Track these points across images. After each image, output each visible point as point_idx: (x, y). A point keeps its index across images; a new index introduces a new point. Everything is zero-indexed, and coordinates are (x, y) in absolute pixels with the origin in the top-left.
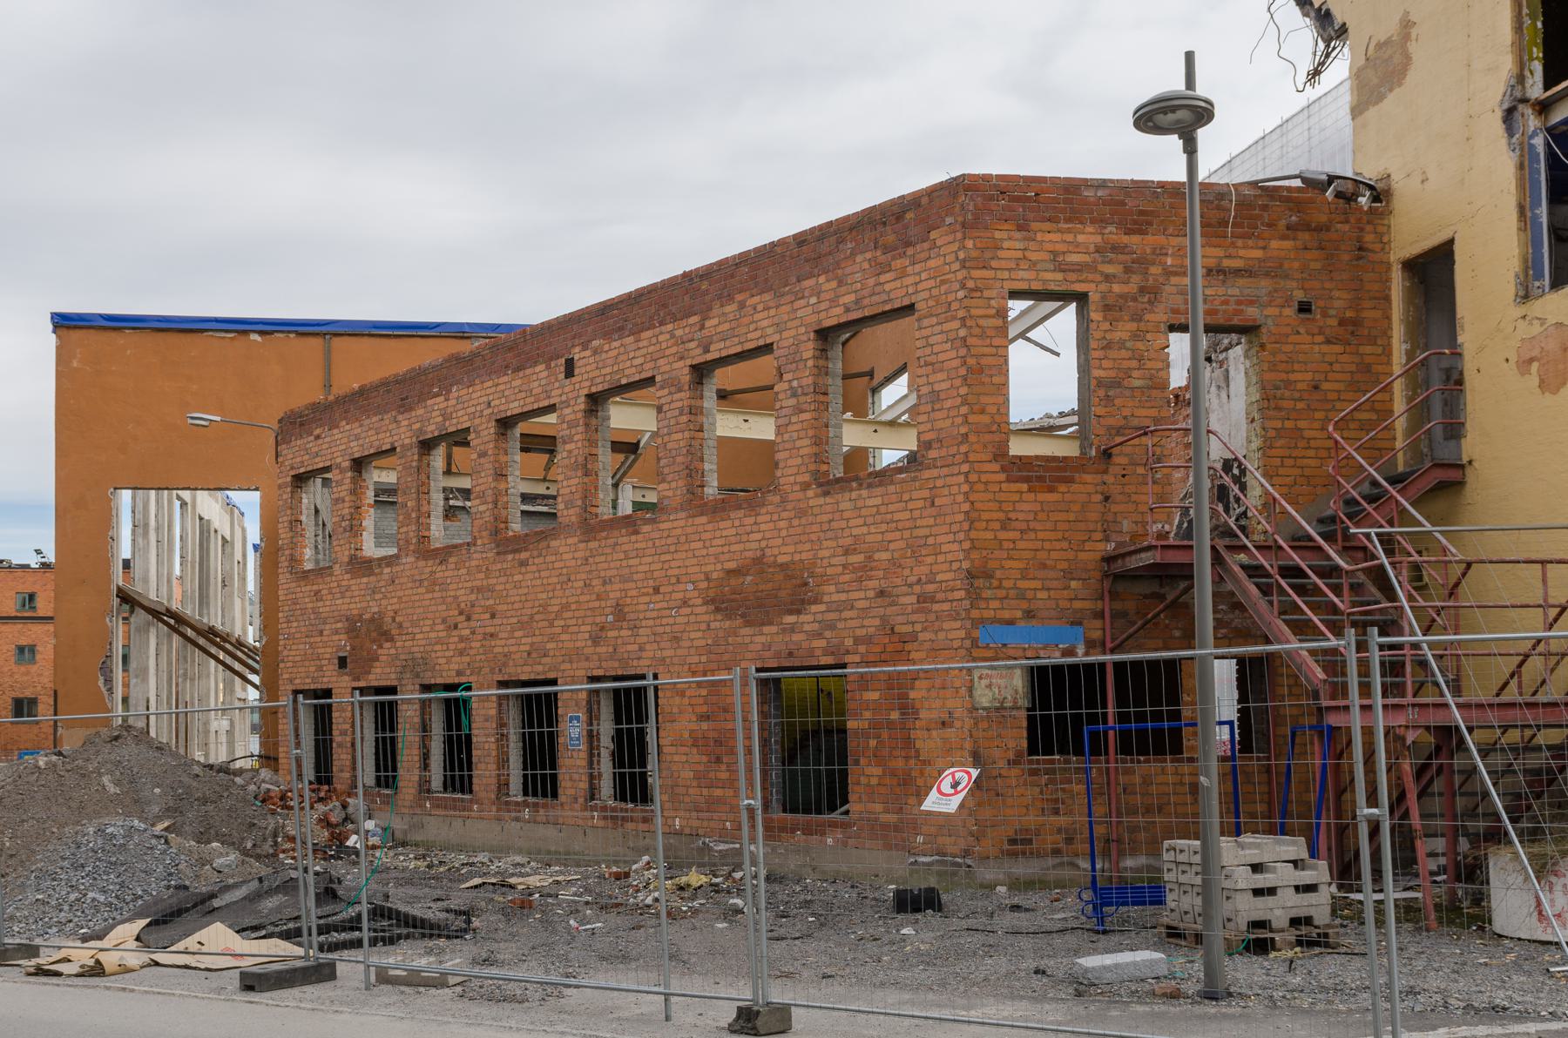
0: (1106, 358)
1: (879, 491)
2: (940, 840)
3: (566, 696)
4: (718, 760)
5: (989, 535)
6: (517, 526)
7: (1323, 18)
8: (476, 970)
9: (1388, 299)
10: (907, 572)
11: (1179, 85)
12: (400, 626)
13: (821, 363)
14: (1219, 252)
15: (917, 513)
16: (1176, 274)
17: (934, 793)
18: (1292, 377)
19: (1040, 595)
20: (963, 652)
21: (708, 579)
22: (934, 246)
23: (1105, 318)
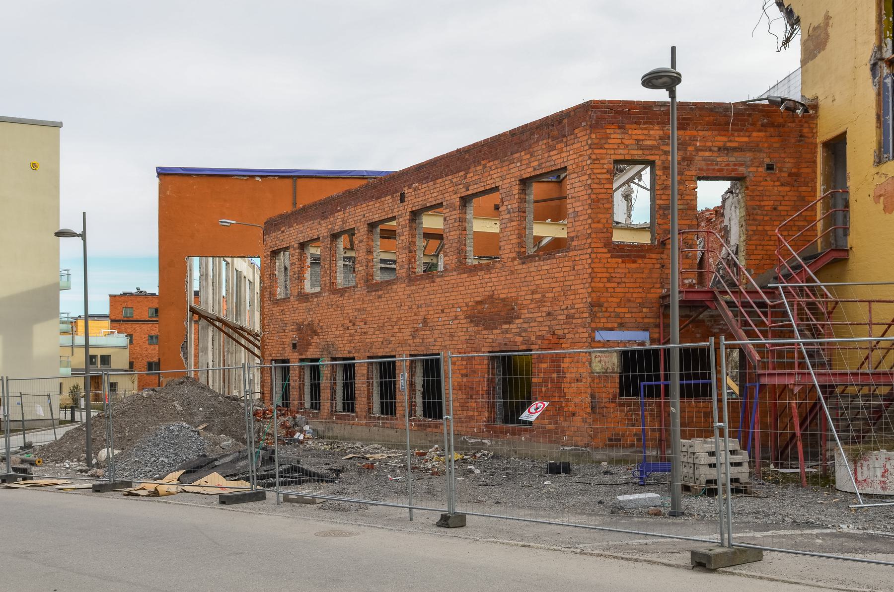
0: (664, 194)
1: (548, 262)
2: (575, 438)
4: (471, 397)
5: (601, 285)
6: (378, 277)
7: (789, 13)
8: (334, 497)
9: (815, 162)
10: (561, 303)
11: (668, 65)
12: (322, 328)
13: (522, 196)
14: (725, 139)
15: (566, 274)
16: (702, 150)
17: (526, 412)
18: (763, 203)
19: (627, 316)
20: (587, 344)
21: (467, 306)
22: (576, 137)
23: (664, 174)
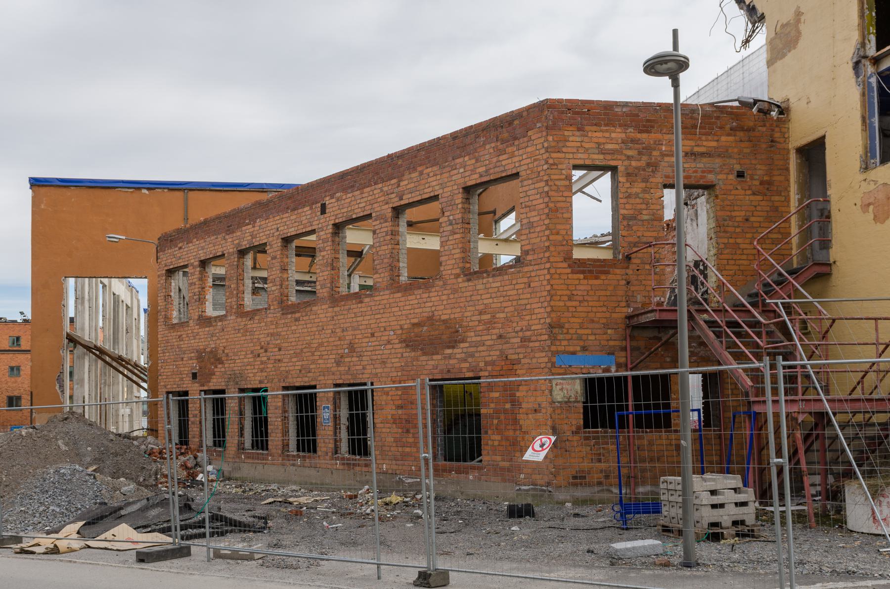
0: (628, 203)
1: (499, 278)
2: (534, 477)
3: (321, 395)
4: (408, 431)
5: (562, 304)
6: (293, 299)
7: (751, 10)
8: (270, 551)
9: (788, 169)
10: (515, 325)
11: (669, 48)
12: (227, 355)
13: (466, 206)
14: (692, 143)
15: (520, 291)
16: (668, 155)
17: (530, 450)
18: (733, 214)
19: (590, 338)
20: (547, 370)
21: (402, 329)
22: (530, 140)
23: (627, 181)
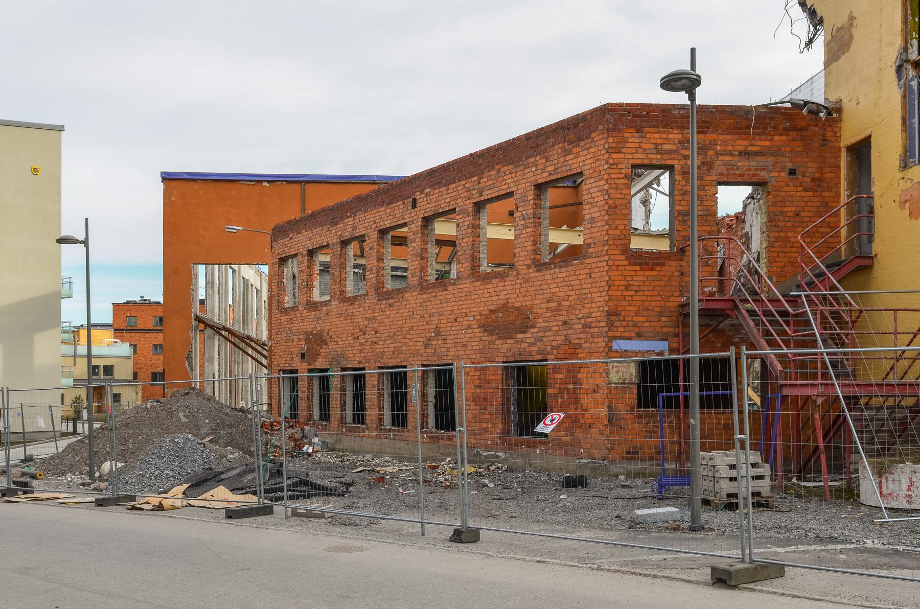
0: (683, 200)
1: (564, 269)
2: (592, 451)
4: (485, 409)
5: (619, 293)
6: (389, 285)
7: (812, 13)
8: (343, 511)
9: (839, 167)
10: (577, 312)
11: (687, 67)
12: (331, 337)
13: (538, 202)
14: (746, 143)
15: (583, 282)
16: (722, 155)
17: (542, 424)
18: (785, 209)
19: (645, 325)
20: (604, 354)
21: (480, 314)
22: (593, 141)
23: (683, 179)
